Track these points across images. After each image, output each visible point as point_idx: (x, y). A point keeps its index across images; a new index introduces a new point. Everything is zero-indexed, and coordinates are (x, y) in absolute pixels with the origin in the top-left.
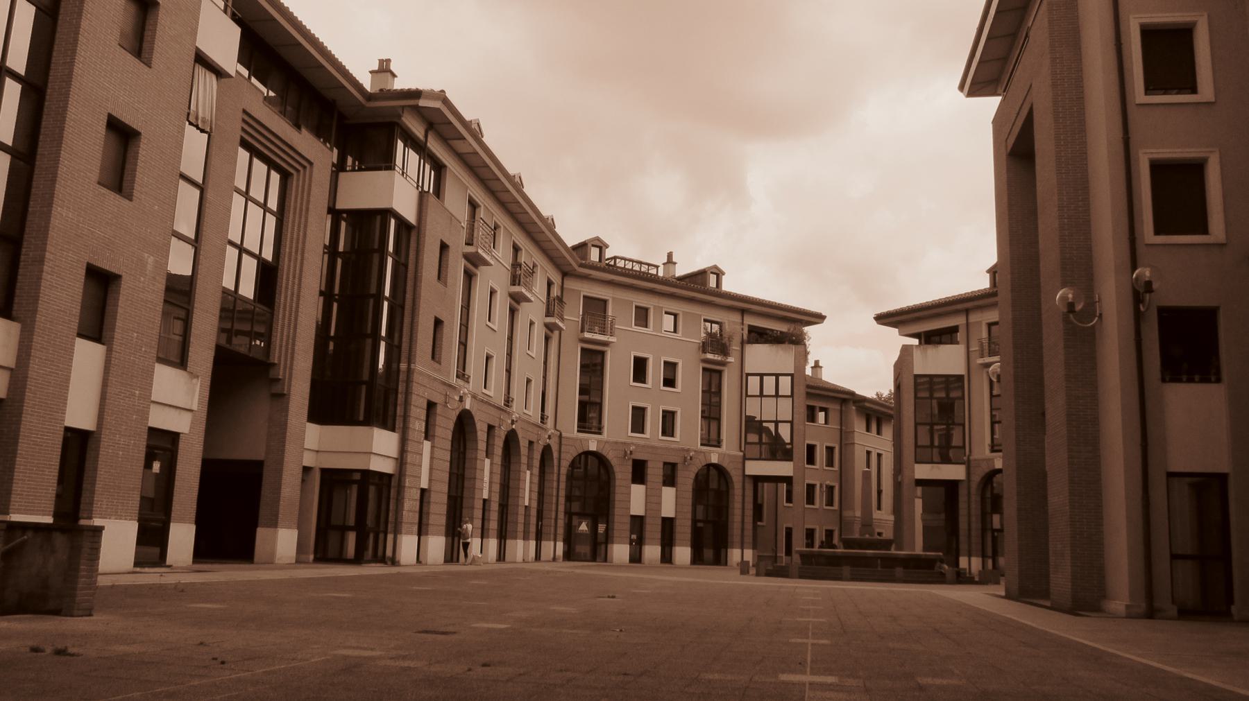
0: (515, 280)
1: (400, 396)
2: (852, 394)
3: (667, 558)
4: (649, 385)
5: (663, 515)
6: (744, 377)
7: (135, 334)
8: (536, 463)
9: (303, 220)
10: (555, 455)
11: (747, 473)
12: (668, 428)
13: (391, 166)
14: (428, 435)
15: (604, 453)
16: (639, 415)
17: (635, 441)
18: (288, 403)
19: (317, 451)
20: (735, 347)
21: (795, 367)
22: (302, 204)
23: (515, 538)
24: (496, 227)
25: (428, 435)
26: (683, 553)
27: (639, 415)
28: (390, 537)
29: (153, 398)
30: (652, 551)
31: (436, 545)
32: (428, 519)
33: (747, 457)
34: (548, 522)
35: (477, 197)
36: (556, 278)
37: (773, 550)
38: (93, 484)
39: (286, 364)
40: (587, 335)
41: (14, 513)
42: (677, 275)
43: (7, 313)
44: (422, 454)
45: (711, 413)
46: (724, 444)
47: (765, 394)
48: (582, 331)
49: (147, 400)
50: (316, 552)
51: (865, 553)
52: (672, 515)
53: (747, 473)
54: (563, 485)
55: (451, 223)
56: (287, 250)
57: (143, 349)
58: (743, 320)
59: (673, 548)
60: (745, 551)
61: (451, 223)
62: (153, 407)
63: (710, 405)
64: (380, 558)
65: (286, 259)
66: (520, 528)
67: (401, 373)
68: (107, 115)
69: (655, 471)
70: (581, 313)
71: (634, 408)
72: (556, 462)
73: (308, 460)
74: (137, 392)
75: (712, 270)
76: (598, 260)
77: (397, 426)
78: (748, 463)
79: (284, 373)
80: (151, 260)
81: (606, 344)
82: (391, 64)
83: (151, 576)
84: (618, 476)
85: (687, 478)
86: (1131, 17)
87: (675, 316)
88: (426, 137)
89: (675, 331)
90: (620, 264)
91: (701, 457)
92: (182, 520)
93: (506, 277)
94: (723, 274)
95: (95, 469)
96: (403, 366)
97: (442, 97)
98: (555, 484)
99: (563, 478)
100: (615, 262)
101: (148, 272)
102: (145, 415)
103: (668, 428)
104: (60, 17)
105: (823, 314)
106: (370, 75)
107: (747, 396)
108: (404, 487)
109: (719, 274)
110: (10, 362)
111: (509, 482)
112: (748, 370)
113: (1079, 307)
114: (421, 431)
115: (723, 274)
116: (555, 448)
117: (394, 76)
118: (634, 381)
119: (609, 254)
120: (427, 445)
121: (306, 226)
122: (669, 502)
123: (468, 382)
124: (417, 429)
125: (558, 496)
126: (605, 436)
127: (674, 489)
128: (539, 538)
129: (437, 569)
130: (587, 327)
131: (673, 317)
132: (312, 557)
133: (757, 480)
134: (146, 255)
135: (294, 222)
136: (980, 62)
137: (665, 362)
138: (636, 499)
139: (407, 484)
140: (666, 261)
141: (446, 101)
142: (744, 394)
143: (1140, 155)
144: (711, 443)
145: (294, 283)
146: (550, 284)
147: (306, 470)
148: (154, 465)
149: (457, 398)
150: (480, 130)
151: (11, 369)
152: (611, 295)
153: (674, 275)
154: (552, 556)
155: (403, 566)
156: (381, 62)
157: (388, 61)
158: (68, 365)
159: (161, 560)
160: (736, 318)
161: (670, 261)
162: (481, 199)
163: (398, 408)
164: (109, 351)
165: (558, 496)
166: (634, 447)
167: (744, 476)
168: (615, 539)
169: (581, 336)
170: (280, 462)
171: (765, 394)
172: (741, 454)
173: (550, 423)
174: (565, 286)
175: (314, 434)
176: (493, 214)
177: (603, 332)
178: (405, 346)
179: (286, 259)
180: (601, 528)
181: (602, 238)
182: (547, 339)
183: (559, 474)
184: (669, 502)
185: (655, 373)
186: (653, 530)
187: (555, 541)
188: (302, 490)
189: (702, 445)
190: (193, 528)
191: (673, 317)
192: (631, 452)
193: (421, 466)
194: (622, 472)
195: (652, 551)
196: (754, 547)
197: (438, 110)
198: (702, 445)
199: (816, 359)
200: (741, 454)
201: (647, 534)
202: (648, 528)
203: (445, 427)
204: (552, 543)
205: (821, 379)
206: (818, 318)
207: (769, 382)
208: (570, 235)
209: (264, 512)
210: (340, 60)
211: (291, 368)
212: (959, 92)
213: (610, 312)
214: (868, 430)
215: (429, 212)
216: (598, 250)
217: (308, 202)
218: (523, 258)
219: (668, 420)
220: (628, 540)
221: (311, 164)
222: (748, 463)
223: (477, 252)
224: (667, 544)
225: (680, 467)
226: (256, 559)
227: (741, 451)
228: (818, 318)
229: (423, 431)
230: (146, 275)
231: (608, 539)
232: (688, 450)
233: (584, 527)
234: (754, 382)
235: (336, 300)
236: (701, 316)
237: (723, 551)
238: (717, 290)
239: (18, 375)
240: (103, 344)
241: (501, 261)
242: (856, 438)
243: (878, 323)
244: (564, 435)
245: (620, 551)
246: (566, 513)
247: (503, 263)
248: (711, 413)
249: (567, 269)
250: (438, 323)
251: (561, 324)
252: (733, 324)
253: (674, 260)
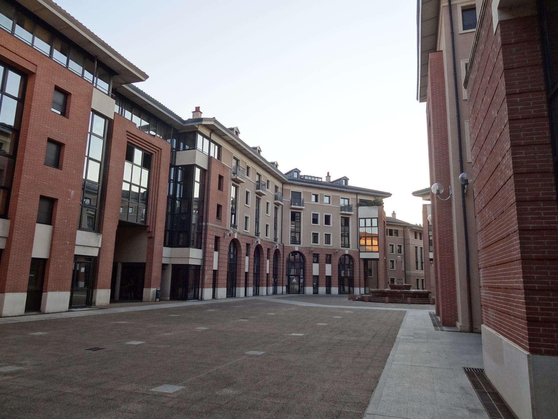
0: (258, 187)
1: (203, 235)
2: (408, 224)
3: (328, 292)
4: (319, 224)
5: (326, 275)
6: (358, 220)
7: (66, 221)
8: (272, 256)
9: (158, 171)
10: (281, 253)
11: (361, 257)
12: (328, 241)
13: (195, 148)
14: (216, 249)
15: (301, 251)
16: (315, 237)
17: (313, 247)
18: (154, 240)
19: (170, 258)
20: (354, 208)
21: (379, 215)
22: (157, 165)
23: (262, 286)
24: (248, 168)
25: (216, 249)
26: (335, 290)
27: (315, 237)
28: (200, 289)
29: (76, 244)
30: (322, 290)
31: (222, 292)
32: (218, 281)
33: (360, 251)
34: (280, 279)
35: (238, 157)
36: (279, 185)
37: (377, 287)
38: (48, 279)
39: (153, 226)
40: (293, 206)
41: (7, 293)
42: (331, 181)
43: (5, 216)
44: (213, 257)
45: (345, 235)
46: (351, 246)
47: (373, 226)
48: (291, 205)
49: (73, 245)
50: (171, 296)
51: (397, 291)
52: (330, 275)
53: (361, 257)
54: (285, 265)
55: (224, 168)
56: (152, 183)
57: (71, 226)
58: (357, 197)
59: (331, 288)
60: (361, 288)
61: (224, 168)
62: (76, 247)
63: (345, 231)
64: (196, 297)
65: (152, 186)
66: (265, 282)
67: (203, 226)
68: (47, 138)
69: (322, 257)
70: (291, 198)
71: (313, 234)
72: (282, 256)
73: (164, 261)
74: (68, 242)
75: (344, 178)
76: (297, 177)
77: (202, 247)
78: (361, 254)
79: (152, 229)
80: (73, 192)
81: (301, 209)
82: (200, 108)
83: (34, 317)
84: (307, 260)
85: (336, 260)
86: (461, 61)
87: (329, 197)
88: (210, 135)
89: (329, 203)
90: (306, 178)
91: (341, 252)
92: (104, 288)
93: (254, 187)
94: (348, 179)
95: (48, 273)
96: (204, 224)
97: (214, 119)
98: (282, 264)
99: (285, 262)
100: (304, 177)
101: (71, 197)
102: (73, 250)
103: (328, 241)
104: (25, 102)
105: (391, 193)
106: (192, 113)
107: (360, 227)
108: (205, 270)
109: (346, 179)
110: (6, 234)
111: (260, 265)
112: (359, 217)
113: (442, 191)
114: (212, 248)
115: (348, 179)
116: (281, 251)
117: (201, 113)
118: (313, 223)
119: (301, 174)
120: (216, 254)
121: (159, 173)
122: (329, 270)
123: (236, 228)
124: (210, 247)
125: (283, 269)
126: (301, 245)
127: (331, 264)
128: (275, 285)
129: (223, 301)
130: (292, 204)
131: (328, 197)
132: (169, 298)
133: (366, 261)
134: (70, 190)
135: (154, 172)
136: (420, 87)
137: (313, 214)
138: (316, 269)
139: (206, 269)
140: (327, 176)
141: (216, 121)
142: (358, 226)
143: (465, 123)
144: (346, 246)
145: (155, 195)
146: (276, 187)
147: (164, 266)
148: (82, 269)
149: (228, 234)
150: (238, 131)
151: (7, 238)
152: (303, 190)
153: (330, 181)
154: (282, 292)
155: (205, 300)
156: (196, 108)
157: (199, 107)
158: (32, 235)
159: (89, 302)
160: (354, 196)
161: (328, 176)
162: (240, 157)
163: (202, 240)
164: (54, 228)
165: (283, 269)
166: (313, 249)
167: (360, 258)
168: (218, 285)
169: (291, 207)
170: (151, 263)
171: (373, 226)
172: (358, 250)
173: (279, 241)
174: (283, 188)
175: (167, 251)
176: (246, 163)
177: (300, 205)
178: (204, 216)
179: (152, 186)
180: (302, 281)
181: (298, 168)
182: (276, 209)
183: (283, 260)
184: (329, 270)
185: (321, 220)
186: (322, 281)
187: (283, 286)
188: (162, 274)
189: (342, 247)
190: (110, 290)
191: (328, 197)
192: (312, 251)
193: (213, 261)
194: (309, 258)
195: (322, 290)
196: (365, 286)
197: (213, 125)
198: (342, 247)
199: (394, 211)
200: (358, 250)
201: (320, 283)
202: (320, 280)
203: (225, 245)
204: (281, 287)
205: (395, 218)
206: (388, 195)
207: (368, 221)
208: (284, 169)
209: (146, 282)
210: (169, 109)
211: (155, 228)
212: (417, 101)
213: (302, 197)
214: (416, 238)
215: (212, 165)
216: (297, 173)
217: (160, 164)
218: (262, 179)
219: (328, 237)
220: (312, 285)
221: (161, 149)
222: (361, 254)
223: (237, 178)
224: (329, 285)
225: (332, 256)
226: (143, 300)
227: (358, 249)
228: (388, 195)
229: (214, 248)
230: (71, 198)
231: (304, 285)
232: (335, 249)
233: (294, 280)
234: (362, 222)
235: (178, 200)
236: (339, 196)
237: (234, 288)
238: (346, 186)
239: (9, 240)
240: (52, 225)
241: (251, 180)
242: (410, 241)
243: (414, 196)
244: (285, 245)
245: (309, 290)
246: (287, 275)
247: (252, 181)
248: (345, 235)
249: (284, 181)
250: (219, 207)
251: (281, 203)
252: (353, 200)
253: (330, 175)
